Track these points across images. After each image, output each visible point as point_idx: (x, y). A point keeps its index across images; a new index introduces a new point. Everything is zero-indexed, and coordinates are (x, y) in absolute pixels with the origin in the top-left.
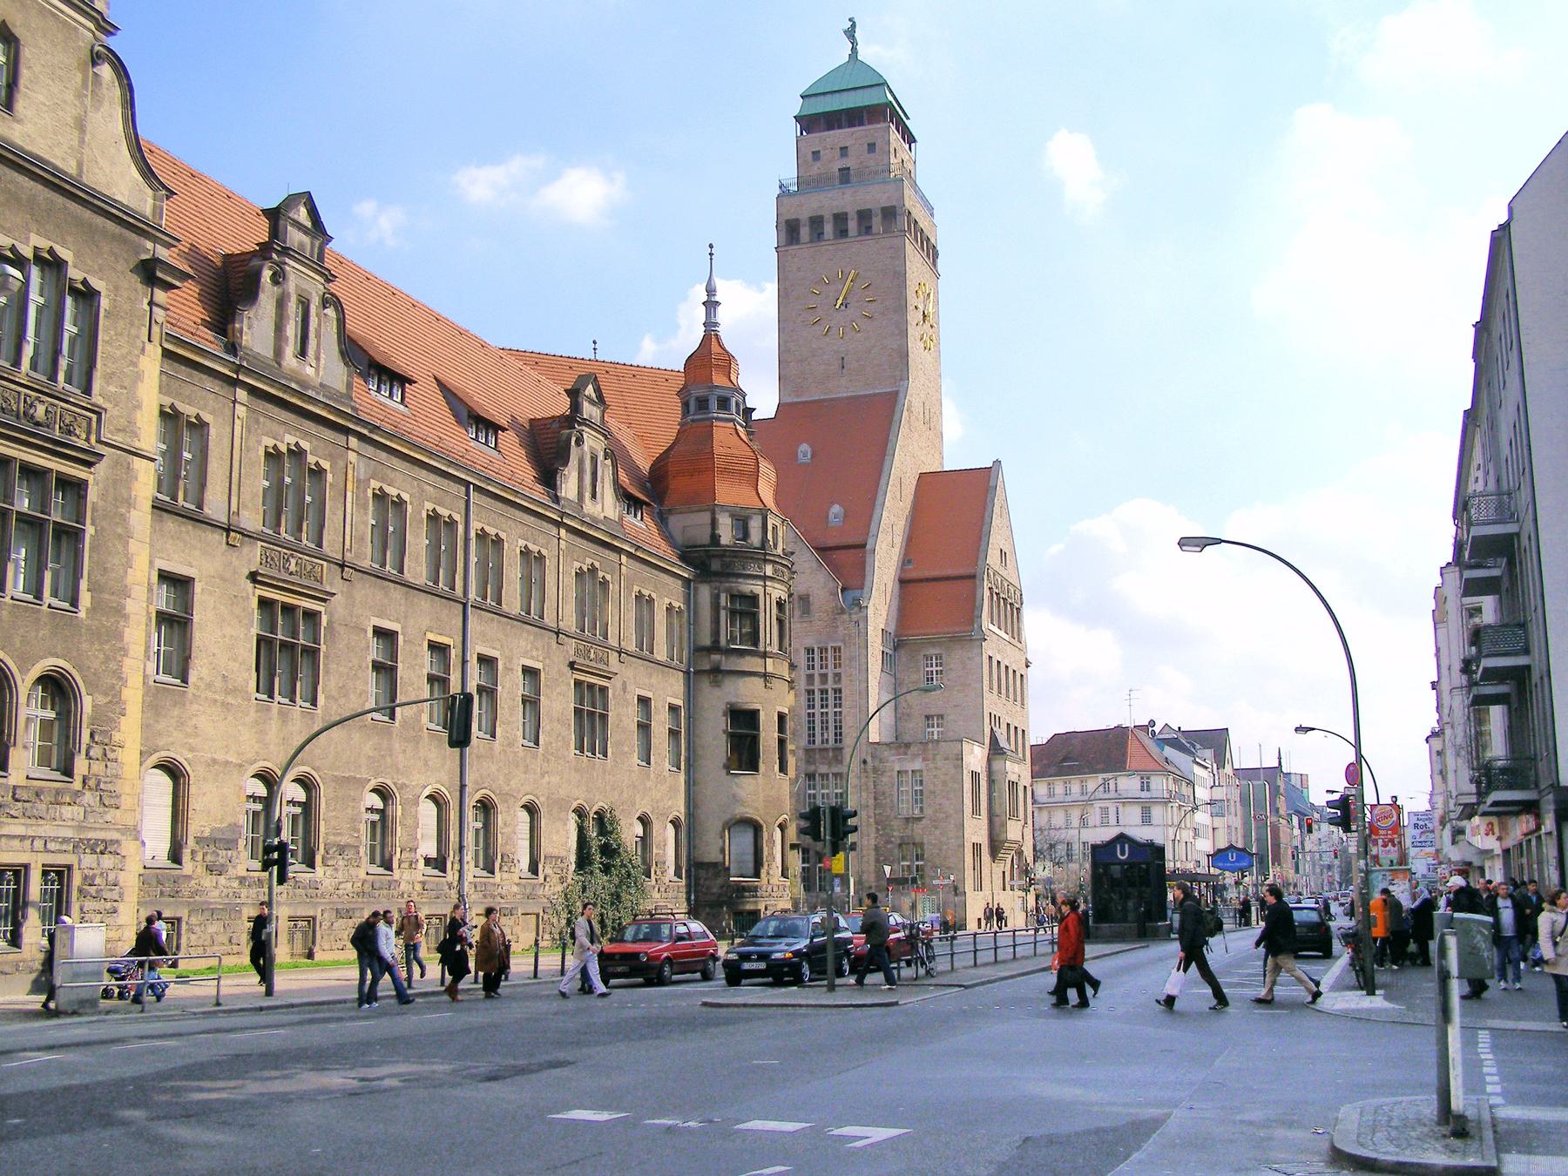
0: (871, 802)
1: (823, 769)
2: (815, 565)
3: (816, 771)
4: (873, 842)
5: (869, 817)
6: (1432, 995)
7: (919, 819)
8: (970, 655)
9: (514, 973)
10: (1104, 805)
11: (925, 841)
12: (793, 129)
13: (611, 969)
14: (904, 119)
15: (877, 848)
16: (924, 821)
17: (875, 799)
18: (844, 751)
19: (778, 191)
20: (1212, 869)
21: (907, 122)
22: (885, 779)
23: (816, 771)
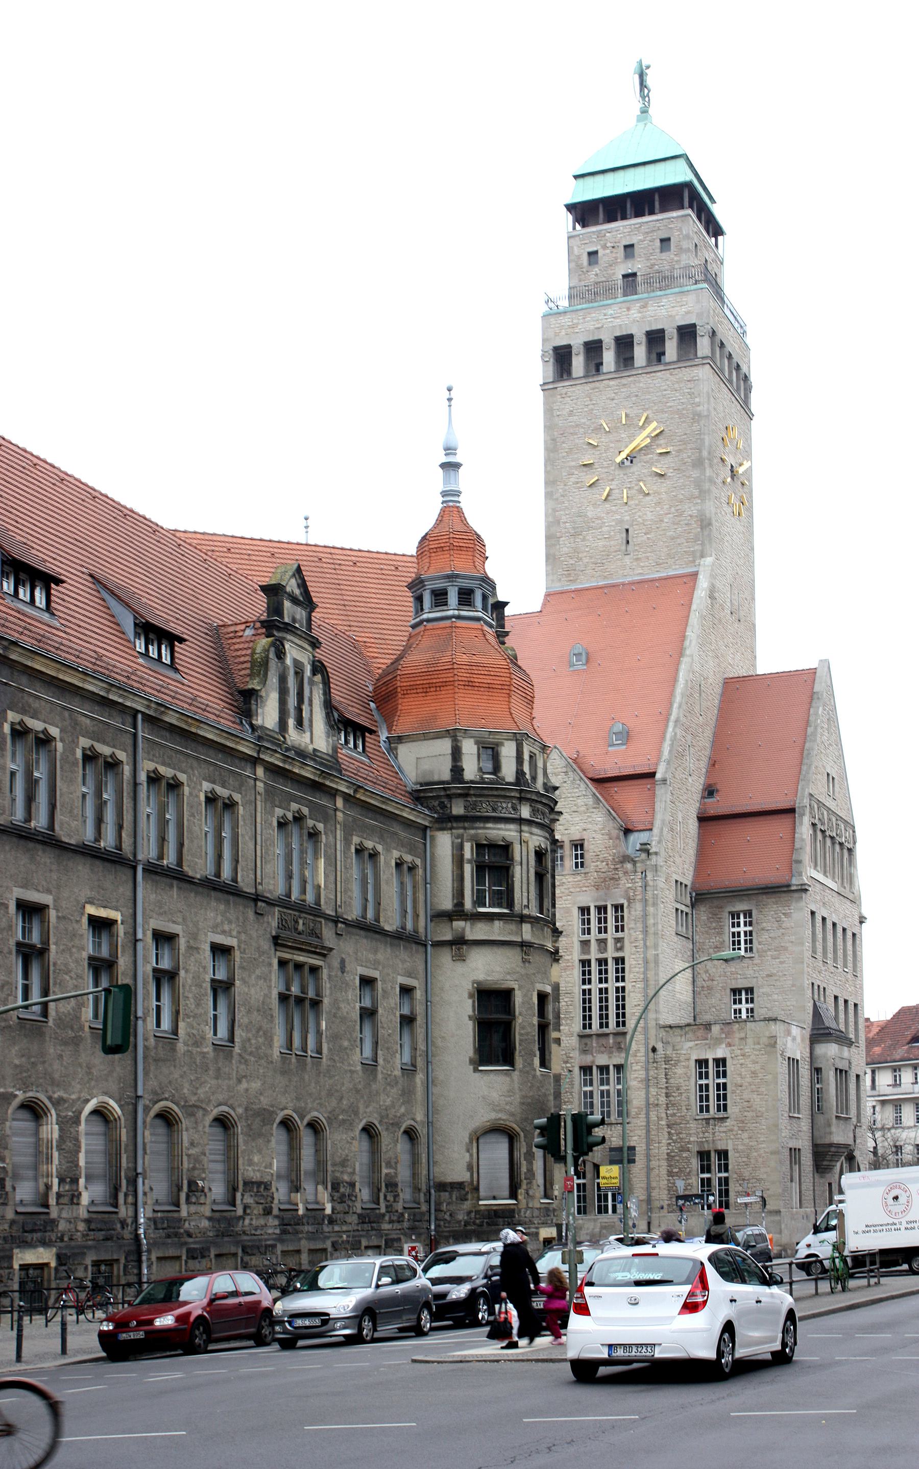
0: (662, 1100)
1: (602, 1060)
3: (593, 1062)
4: (664, 1150)
5: (659, 1119)
11: (730, 1148)
16: (728, 1123)
23: (593, 1062)
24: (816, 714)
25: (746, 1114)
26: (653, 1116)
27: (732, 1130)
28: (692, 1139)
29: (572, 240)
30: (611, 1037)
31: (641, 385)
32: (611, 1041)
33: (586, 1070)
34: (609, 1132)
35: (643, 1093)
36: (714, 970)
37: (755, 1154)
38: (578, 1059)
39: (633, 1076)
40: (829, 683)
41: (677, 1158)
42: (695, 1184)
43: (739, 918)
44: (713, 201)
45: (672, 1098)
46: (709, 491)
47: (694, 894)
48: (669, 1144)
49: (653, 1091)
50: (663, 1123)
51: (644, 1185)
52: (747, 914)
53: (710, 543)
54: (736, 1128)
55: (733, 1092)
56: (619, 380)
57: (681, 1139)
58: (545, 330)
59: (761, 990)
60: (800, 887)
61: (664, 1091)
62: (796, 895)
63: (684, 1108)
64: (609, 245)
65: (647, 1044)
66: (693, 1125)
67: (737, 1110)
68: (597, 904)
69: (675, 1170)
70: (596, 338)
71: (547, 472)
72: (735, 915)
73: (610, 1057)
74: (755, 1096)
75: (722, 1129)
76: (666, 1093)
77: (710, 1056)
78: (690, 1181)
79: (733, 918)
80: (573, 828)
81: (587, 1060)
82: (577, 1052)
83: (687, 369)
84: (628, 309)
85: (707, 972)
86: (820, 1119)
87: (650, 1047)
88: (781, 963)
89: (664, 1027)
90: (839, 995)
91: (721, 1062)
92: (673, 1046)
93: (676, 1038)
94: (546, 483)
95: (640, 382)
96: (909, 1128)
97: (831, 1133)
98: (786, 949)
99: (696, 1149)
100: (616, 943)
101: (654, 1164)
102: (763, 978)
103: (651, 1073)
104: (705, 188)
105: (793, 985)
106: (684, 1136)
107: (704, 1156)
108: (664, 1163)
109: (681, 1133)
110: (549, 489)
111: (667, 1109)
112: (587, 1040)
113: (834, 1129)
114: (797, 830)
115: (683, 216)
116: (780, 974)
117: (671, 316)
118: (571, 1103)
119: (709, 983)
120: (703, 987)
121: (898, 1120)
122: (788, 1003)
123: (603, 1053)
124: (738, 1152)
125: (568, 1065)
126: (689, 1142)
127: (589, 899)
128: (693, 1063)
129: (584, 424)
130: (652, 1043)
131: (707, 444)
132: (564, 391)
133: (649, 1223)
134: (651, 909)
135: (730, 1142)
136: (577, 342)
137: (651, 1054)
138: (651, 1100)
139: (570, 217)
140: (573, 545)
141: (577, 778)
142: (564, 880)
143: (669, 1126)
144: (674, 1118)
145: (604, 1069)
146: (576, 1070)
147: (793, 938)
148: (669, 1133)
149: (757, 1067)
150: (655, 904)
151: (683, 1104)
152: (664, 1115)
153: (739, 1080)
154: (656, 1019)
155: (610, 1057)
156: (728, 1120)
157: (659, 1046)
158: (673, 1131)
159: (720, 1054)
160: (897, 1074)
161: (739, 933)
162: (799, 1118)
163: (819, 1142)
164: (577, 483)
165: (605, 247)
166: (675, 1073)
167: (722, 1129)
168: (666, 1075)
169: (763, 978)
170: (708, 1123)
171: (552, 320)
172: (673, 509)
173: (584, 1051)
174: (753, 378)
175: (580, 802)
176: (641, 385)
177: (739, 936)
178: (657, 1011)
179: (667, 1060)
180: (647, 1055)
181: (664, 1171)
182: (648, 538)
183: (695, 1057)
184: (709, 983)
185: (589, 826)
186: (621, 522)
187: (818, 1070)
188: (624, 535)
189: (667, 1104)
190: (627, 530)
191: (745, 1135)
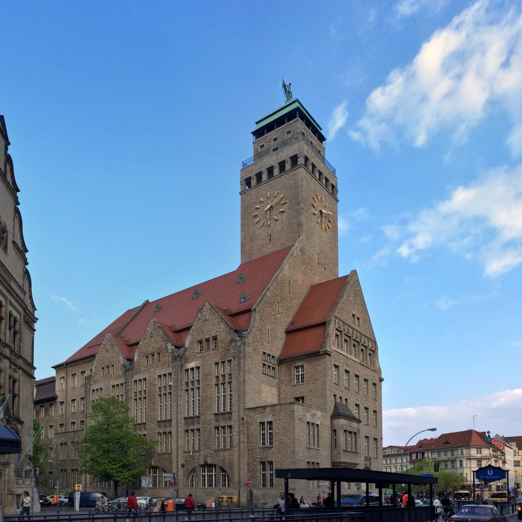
0: (246, 439)
1: (223, 424)
2: (220, 320)
3: (219, 425)
4: (246, 461)
5: (244, 448)
6: (460, 451)
7: (271, 448)
8: (318, 363)
9: (361, 485)
10: (461, 460)
11: (273, 460)
12: (252, 138)
13: (475, 473)
14: (319, 130)
15: (249, 464)
16: (273, 449)
17: (248, 438)
18: (233, 414)
19: (241, 167)
20: (476, 480)
21: (321, 131)
22: (253, 428)
23: (219, 425)
24: (346, 288)
25: (281, 445)
26: (242, 446)
27: (274, 453)
28: (257, 456)
29: (255, 144)
30: (226, 414)
31: (276, 182)
32: (226, 416)
33: (217, 428)
34: (225, 454)
35: (237, 437)
36: (288, 391)
37: (285, 463)
38: (214, 424)
39: (234, 430)
40: (357, 280)
41: (251, 464)
42: (259, 476)
43: (299, 369)
44: (321, 129)
45: (250, 439)
46: (302, 212)
47: (278, 360)
48: (248, 458)
49: (242, 436)
50: (246, 449)
51: (238, 476)
52: (302, 366)
53: (302, 232)
54: (276, 452)
55: (275, 436)
56: (268, 183)
57: (253, 456)
58: (241, 174)
59: (307, 397)
60: (324, 352)
61: (246, 436)
62: (323, 356)
63: (254, 443)
64: (268, 141)
65: (239, 416)
66: (258, 450)
67: (277, 444)
68: (222, 361)
69: (251, 470)
70: (260, 171)
71: (241, 222)
72: (297, 368)
73: (226, 423)
74: (285, 438)
75: (270, 452)
76: (247, 437)
77: (265, 420)
78: (257, 475)
79: (297, 369)
80: (213, 332)
81: (217, 424)
82: (214, 422)
83: (294, 171)
84: (272, 157)
85: (284, 391)
86: (335, 451)
87: (241, 418)
88: (316, 385)
89: (247, 409)
90: (342, 396)
91: (270, 423)
92: (250, 417)
93: (252, 414)
94: (241, 226)
95: (275, 181)
96: (449, 469)
97: (340, 457)
98: (318, 379)
99: (259, 460)
100: (229, 376)
101: (242, 467)
102: (308, 392)
103: (241, 429)
104: (307, 112)
105: (321, 395)
106: (255, 455)
107: (263, 463)
108: (246, 466)
109: (253, 454)
110: (243, 228)
111: (248, 443)
112: (217, 416)
113: (341, 456)
114: (327, 330)
115: (295, 121)
116: (316, 390)
117: (288, 154)
118: (211, 442)
119: (286, 396)
120: (283, 398)
121: (446, 466)
122: (319, 402)
123: (223, 421)
124: (277, 462)
125: (210, 427)
126: (256, 458)
127: (219, 359)
128: (258, 424)
129: (255, 202)
130: (242, 416)
131: (301, 196)
132: (248, 192)
133: (239, 492)
134: (242, 361)
135: (274, 458)
136: (253, 174)
137: (241, 421)
138: (241, 440)
139: (253, 135)
140: (251, 246)
141: (215, 311)
142: (210, 353)
143: (248, 451)
144: (251, 448)
145: (224, 427)
146: (213, 429)
147: (321, 375)
148: (248, 454)
149: (286, 424)
150: (244, 358)
151: (254, 441)
152: (246, 446)
153: (278, 431)
154: (244, 406)
155: (226, 423)
156: (273, 448)
157: (245, 417)
158: (250, 453)
159: (269, 420)
160: (446, 452)
161: (299, 375)
162: (319, 450)
163: (334, 461)
164: (252, 223)
165: (266, 142)
166: (251, 428)
167: (270, 452)
168: (247, 429)
169: (308, 392)
170: (264, 450)
171: (244, 170)
172: (288, 223)
173: (217, 421)
174: (339, 187)
175: (216, 321)
176: (276, 182)
177: (299, 376)
178: (244, 403)
179: (248, 423)
180: (239, 421)
181: (246, 470)
182: (278, 236)
183: (259, 421)
184: (286, 396)
185: (219, 330)
186: (268, 232)
187: (335, 431)
188: (269, 237)
189: (248, 442)
190: (270, 235)
191: (280, 455)
